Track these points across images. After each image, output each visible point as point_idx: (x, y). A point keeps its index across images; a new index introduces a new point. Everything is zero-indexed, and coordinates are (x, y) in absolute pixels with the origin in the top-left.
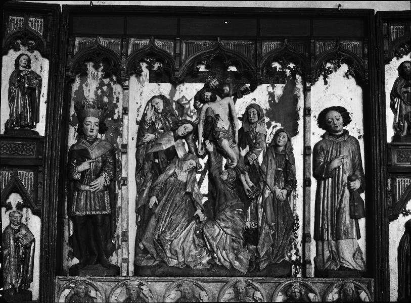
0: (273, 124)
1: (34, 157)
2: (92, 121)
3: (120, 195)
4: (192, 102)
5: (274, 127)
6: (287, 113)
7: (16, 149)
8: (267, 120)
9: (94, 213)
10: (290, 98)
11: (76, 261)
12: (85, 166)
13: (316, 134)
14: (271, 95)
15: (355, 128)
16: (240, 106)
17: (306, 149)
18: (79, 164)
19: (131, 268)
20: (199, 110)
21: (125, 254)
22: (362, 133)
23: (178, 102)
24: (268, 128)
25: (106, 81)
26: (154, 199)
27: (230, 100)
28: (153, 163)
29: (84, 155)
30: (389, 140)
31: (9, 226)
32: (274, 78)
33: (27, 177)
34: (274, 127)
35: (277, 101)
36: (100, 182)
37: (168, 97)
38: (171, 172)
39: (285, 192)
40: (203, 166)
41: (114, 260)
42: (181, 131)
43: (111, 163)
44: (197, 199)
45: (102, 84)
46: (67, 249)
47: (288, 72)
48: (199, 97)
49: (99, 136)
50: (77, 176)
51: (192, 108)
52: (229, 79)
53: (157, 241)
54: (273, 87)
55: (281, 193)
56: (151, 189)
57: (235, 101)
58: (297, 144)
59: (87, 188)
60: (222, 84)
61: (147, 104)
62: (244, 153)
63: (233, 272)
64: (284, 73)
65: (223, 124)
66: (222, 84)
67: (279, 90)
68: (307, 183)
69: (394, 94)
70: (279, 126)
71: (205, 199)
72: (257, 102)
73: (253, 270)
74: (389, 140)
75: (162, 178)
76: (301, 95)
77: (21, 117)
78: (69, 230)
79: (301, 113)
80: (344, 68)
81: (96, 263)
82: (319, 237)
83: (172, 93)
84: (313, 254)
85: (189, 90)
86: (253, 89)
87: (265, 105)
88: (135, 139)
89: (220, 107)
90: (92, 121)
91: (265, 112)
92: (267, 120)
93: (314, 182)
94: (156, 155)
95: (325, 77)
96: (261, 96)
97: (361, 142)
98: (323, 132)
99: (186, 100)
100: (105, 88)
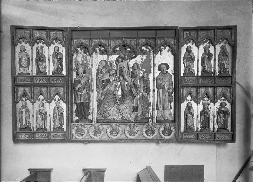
0: (143, 69)
1: (63, 83)
2: (81, 70)
3: (91, 96)
4: (115, 62)
5: (143, 71)
6: (147, 65)
7: (57, 80)
8: (140, 68)
9: (83, 102)
10: (148, 60)
11: (77, 118)
12: (79, 86)
13: (157, 73)
14: (142, 59)
15: (171, 70)
16: (131, 63)
17: (154, 78)
18: (77, 85)
19: (96, 120)
20: (117, 65)
21: (93, 116)
22: (173, 72)
23: (110, 62)
24: (141, 71)
25: (85, 55)
26: (103, 97)
27: (127, 61)
28: (103, 84)
29: (79, 82)
30: (182, 75)
31: (56, 106)
32: (143, 52)
33: (61, 90)
34: (143, 71)
35: (144, 61)
36: (85, 91)
37: (106, 60)
38: (108, 87)
39: (147, 94)
40: (119, 85)
41: (90, 117)
42: (111, 73)
43: (88, 85)
44: (117, 97)
45: (83, 56)
46: (74, 114)
47: (148, 50)
48: (117, 60)
49: (83, 75)
50: (77, 89)
51: (115, 64)
52: (127, 54)
53: (83, 115)
54: (143, 56)
55: (145, 94)
56: (102, 93)
57: (129, 61)
58: (151, 77)
59: (81, 93)
60: (125, 55)
61: (100, 63)
62: (133, 80)
63: (129, 121)
64: (146, 51)
65: (125, 70)
66: (125, 55)
67: (145, 57)
68: (154, 91)
69: (184, 58)
70: (145, 70)
71: (120, 97)
72: (137, 62)
73: (136, 120)
74: (182, 75)
75: (105, 90)
76: (153, 59)
77: (57, 69)
78: (75, 107)
79: (152, 65)
80: (168, 48)
81: (84, 119)
82: (158, 109)
83: (108, 59)
84: (155, 115)
85: (114, 57)
86: (135, 57)
87: (140, 63)
88: (96, 76)
89: (124, 64)
90: (81, 70)
91: (140, 65)
92: (140, 68)
93: (156, 90)
94: (103, 81)
95: (161, 53)
96: (138, 59)
97: (173, 76)
98: (160, 72)
99: (113, 61)
100: (85, 57)
